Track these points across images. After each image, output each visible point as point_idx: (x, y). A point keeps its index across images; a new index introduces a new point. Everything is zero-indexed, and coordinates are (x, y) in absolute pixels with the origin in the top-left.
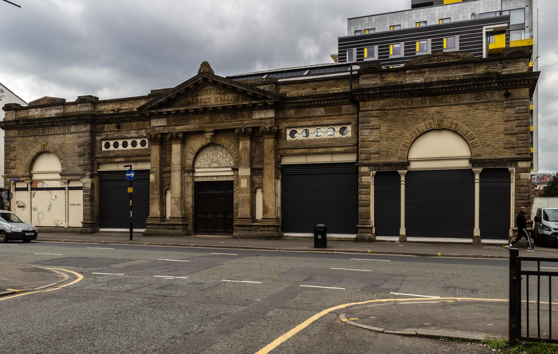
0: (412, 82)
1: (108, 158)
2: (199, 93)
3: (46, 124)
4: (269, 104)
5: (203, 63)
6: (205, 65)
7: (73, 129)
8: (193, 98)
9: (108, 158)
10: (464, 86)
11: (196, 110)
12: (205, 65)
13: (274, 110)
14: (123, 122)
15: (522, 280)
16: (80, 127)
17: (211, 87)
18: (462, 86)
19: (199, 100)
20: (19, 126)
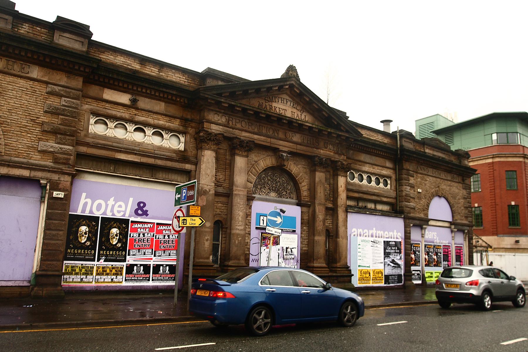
0: (159, 124)
1: (276, 145)
2: (274, 98)
3: (377, 152)
4: (209, 101)
5: (291, 65)
6: (292, 69)
7: (35, 72)
8: (265, 102)
9: (276, 145)
10: (145, 87)
11: (244, 111)
12: (292, 69)
13: (91, 133)
14: (143, 96)
15: (352, 277)
16: (38, 68)
17: (288, 98)
18: (143, 86)
19: (273, 108)
20: (365, 149)
